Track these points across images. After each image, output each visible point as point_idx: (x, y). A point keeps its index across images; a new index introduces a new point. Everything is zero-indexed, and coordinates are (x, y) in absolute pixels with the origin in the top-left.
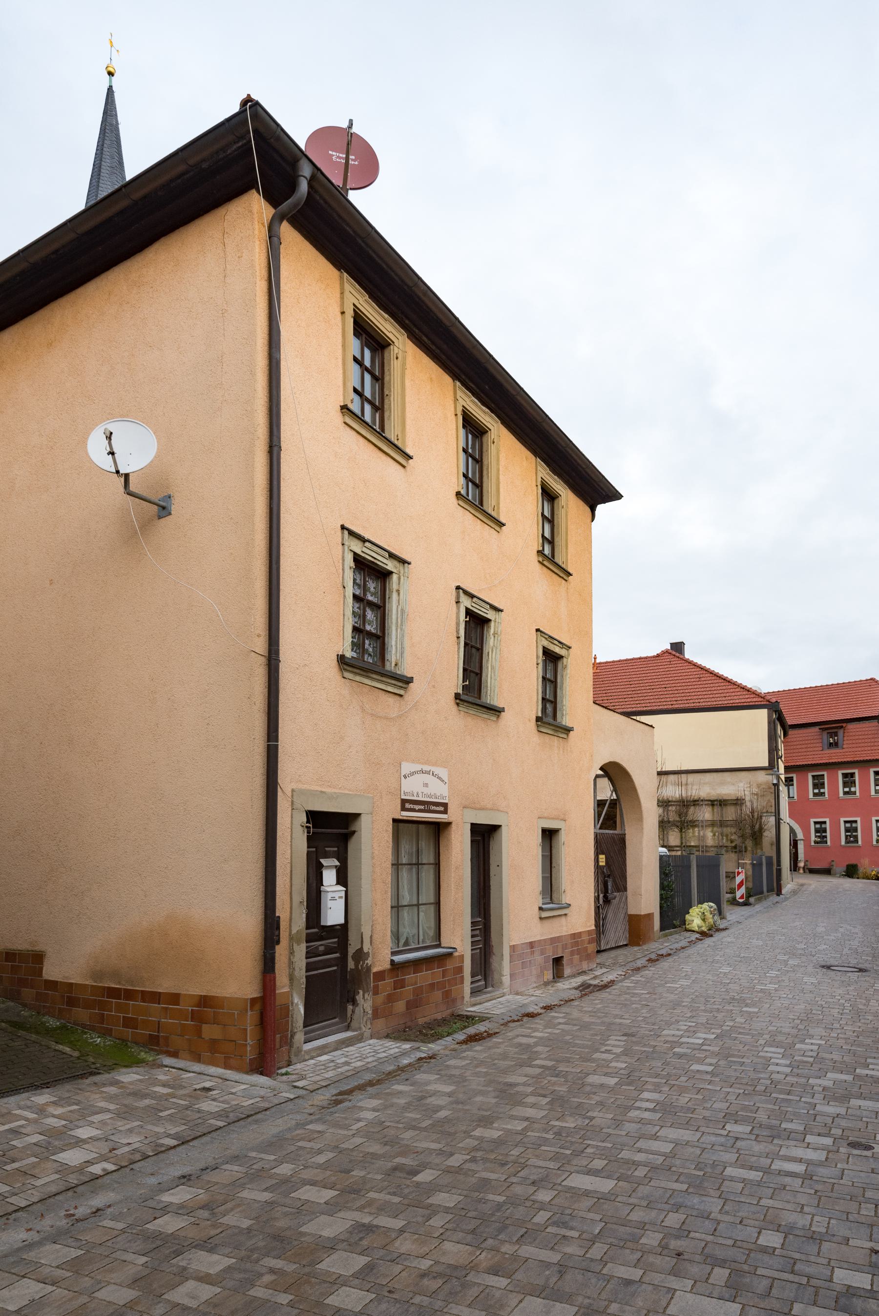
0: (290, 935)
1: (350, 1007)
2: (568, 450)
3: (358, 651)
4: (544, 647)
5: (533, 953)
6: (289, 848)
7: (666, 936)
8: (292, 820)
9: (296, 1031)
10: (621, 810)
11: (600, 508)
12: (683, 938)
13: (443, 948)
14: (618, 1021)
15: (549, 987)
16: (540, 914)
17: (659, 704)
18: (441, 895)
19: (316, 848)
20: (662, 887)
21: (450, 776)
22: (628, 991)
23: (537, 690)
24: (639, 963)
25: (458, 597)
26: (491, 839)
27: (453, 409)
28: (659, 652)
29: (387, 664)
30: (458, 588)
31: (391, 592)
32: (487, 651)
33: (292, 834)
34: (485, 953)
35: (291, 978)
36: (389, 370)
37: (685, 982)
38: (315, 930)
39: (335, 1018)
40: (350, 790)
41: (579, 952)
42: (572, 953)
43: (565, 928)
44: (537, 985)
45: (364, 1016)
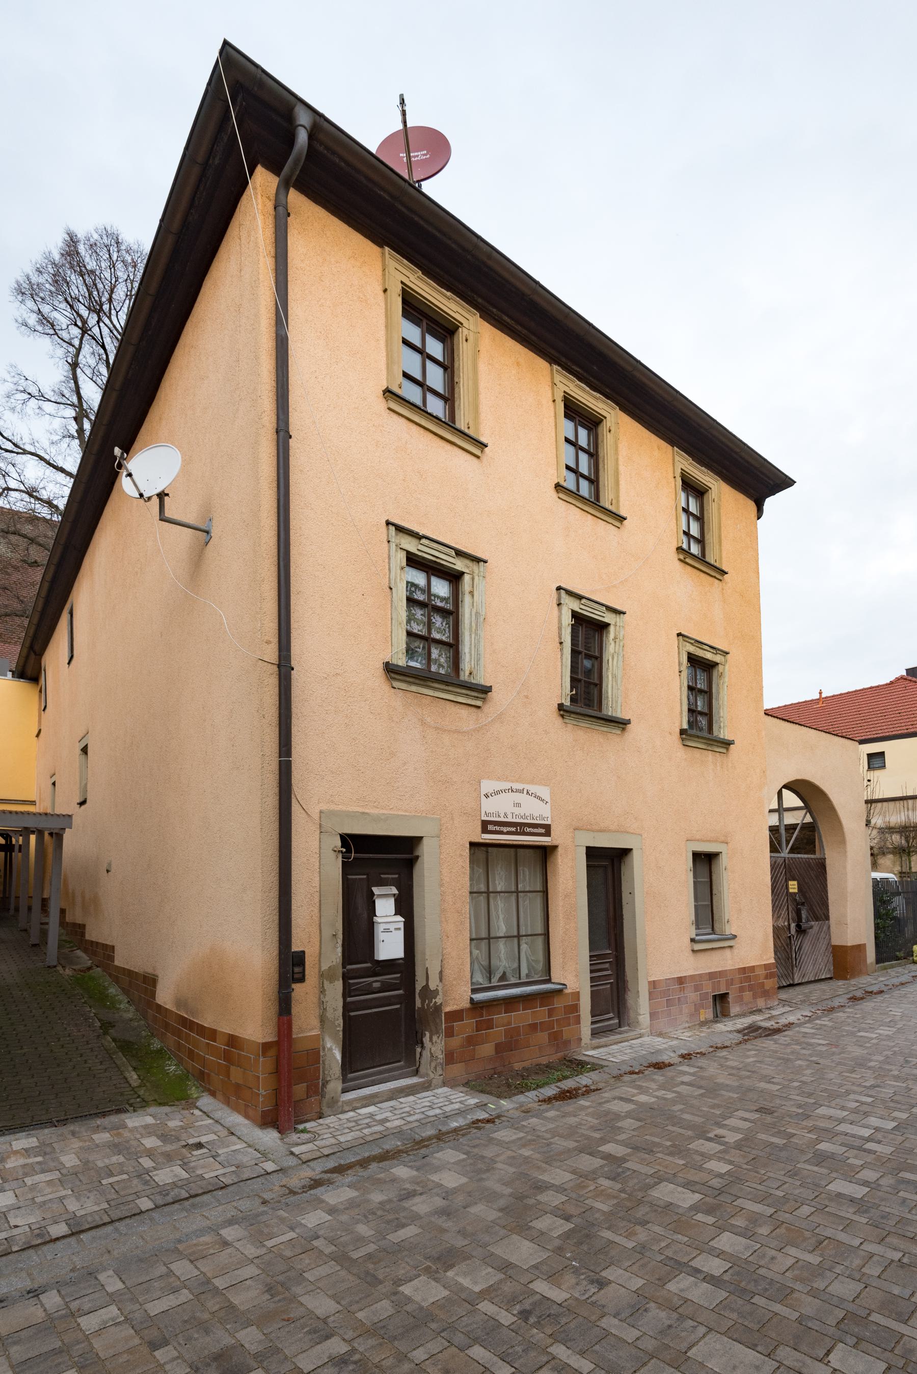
0: (319, 972)
1: (418, 1050)
2: (637, 374)
3: (424, 662)
4: (689, 653)
5: (682, 990)
6: (317, 875)
7: (885, 968)
8: (320, 845)
9: (328, 1079)
10: (819, 833)
11: (770, 503)
12: (907, 972)
13: (554, 983)
14: (763, 1085)
15: (704, 1029)
16: (692, 946)
17: (892, 730)
18: (550, 926)
19: (367, 875)
20: (877, 915)
21: (552, 794)
22: (802, 1040)
23: (681, 700)
24: (836, 1002)
25: (559, 598)
26: (622, 864)
27: (550, 395)
28: (892, 679)
29: (461, 673)
30: (559, 589)
31: (463, 594)
32: (606, 659)
33: (320, 859)
34: (618, 988)
35: (323, 1019)
36: (458, 355)
37: (885, 1031)
38: (369, 965)
39: (399, 1061)
40: (406, 811)
41: (751, 988)
42: (742, 989)
43: (730, 962)
44: (690, 1025)
45: (431, 1061)
